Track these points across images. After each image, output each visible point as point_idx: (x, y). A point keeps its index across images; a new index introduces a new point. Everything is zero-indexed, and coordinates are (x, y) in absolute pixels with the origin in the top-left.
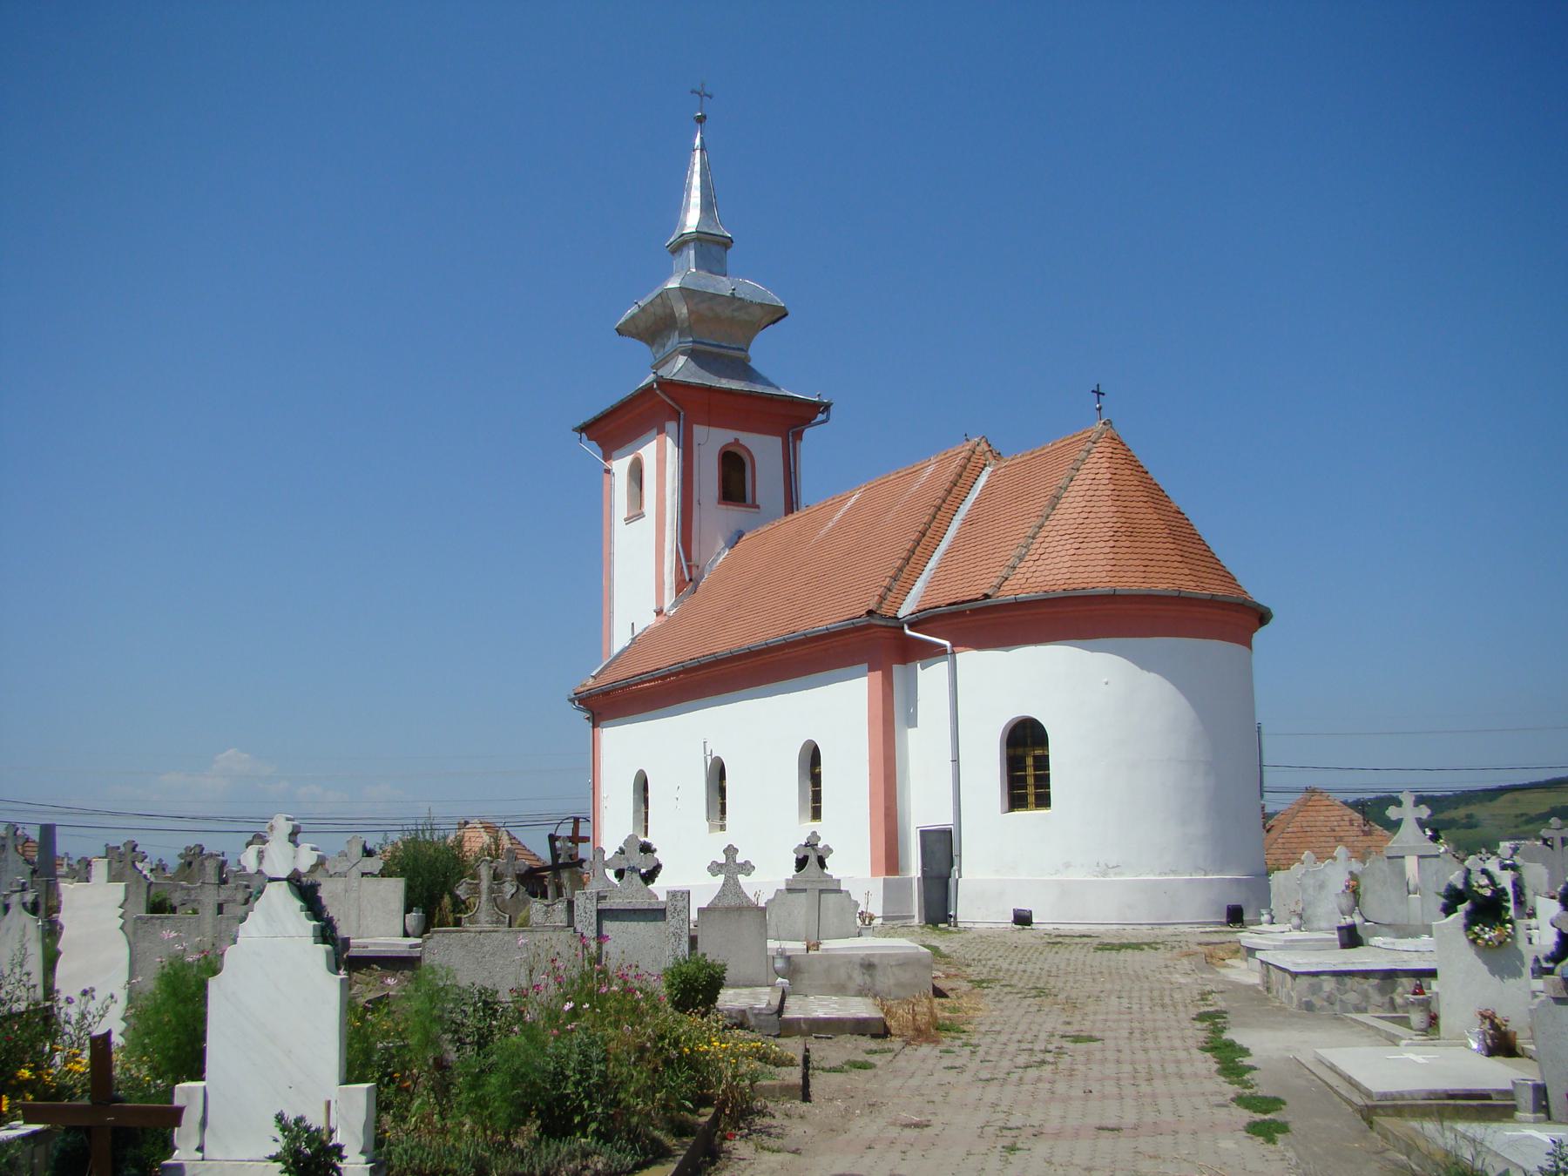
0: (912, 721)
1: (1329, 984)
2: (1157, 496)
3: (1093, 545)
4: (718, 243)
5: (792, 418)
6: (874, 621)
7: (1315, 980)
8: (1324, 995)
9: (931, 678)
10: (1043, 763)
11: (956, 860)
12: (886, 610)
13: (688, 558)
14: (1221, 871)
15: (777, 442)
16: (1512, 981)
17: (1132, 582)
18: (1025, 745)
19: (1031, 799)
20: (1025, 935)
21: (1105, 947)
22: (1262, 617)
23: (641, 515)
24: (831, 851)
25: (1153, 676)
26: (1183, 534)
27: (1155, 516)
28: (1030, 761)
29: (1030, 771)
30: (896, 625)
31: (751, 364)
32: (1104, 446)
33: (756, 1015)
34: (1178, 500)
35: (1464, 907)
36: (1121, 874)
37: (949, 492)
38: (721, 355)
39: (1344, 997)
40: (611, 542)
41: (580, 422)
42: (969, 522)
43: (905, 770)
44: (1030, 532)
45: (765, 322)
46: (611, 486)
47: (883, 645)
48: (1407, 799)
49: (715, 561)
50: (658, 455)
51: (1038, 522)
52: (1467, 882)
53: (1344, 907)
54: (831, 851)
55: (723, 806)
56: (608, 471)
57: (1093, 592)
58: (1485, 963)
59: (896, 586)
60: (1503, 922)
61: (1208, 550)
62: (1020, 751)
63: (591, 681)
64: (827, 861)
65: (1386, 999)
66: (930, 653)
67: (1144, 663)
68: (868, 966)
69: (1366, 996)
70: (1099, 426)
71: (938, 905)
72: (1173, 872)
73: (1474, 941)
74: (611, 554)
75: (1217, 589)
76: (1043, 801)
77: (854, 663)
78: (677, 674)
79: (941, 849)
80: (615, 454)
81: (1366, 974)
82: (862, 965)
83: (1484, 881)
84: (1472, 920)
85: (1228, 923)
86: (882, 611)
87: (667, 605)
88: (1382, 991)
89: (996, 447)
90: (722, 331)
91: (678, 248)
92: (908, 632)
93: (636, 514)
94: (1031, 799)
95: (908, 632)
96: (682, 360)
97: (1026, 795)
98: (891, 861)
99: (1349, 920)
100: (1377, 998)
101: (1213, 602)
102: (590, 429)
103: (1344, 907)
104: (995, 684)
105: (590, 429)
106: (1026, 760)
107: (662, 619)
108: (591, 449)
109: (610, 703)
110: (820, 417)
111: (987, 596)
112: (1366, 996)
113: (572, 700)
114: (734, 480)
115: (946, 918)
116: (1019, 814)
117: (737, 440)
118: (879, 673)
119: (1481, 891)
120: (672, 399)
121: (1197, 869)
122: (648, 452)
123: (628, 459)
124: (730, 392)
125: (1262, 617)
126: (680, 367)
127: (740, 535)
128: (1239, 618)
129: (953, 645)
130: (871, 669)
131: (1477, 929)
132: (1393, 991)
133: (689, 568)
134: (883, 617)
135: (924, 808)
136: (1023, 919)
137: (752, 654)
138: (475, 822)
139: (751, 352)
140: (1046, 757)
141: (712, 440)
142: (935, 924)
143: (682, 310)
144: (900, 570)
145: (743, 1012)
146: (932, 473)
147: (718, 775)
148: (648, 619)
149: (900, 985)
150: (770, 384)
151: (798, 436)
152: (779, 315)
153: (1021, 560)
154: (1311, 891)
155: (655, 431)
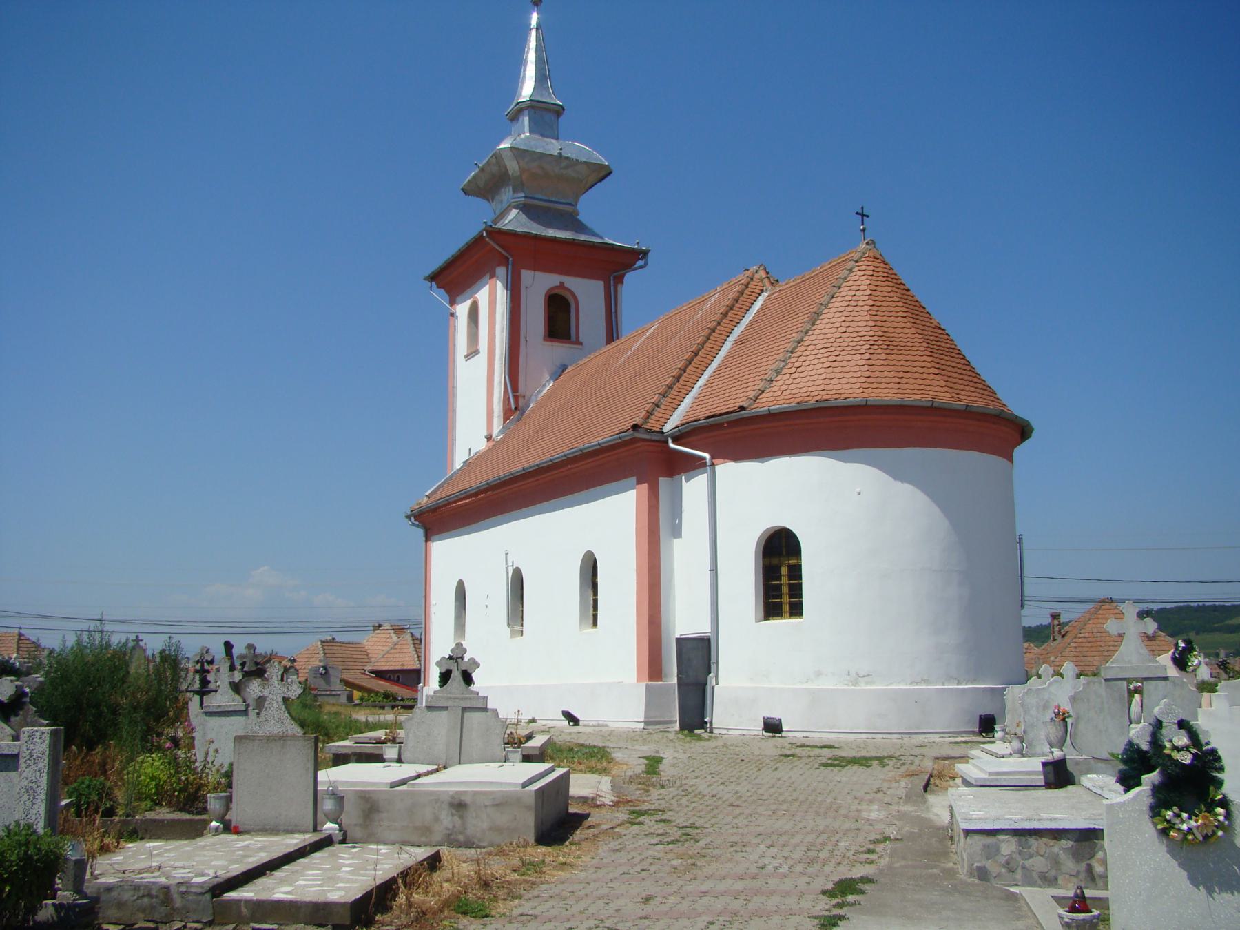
0: (677, 532)
1: (1008, 846)
2: (916, 311)
3: (849, 358)
4: (549, 110)
5: (613, 264)
6: (637, 435)
7: (989, 840)
8: (1003, 860)
9: (693, 489)
10: (796, 572)
12: (652, 424)
14: (974, 681)
15: (599, 286)
16: (1226, 896)
17: (886, 392)
18: (780, 555)
19: (786, 608)
20: (777, 740)
21: (842, 762)
22: (1023, 431)
23: (476, 352)
24: (478, 665)
25: (907, 487)
26: (941, 348)
27: (913, 331)
28: (784, 570)
29: (785, 580)
30: (660, 440)
31: (579, 217)
32: (866, 265)
33: (183, 894)
34: (938, 317)
35: (1151, 778)
37: (725, 315)
38: (549, 209)
39: (1028, 863)
40: (454, 377)
41: (428, 273)
42: (740, 342)
43: (671, 580)
44: (789, 347)
45: (591, 180)
46: (455, 327)
47: (649, 459)
48: (1130, 611)
49: (540, 391)
50: (491, 297)
51: (796, 337)
52: (1155, 741)
53: (1052, 737)
54: (478, 665)
56: (452, 315)
57: (845, 403)
58: (1182, 865)
59: (664, 402)
60: (1211, 805)
61: (972, 370)
62: (775, 561)
63: (425, 499)
64: (474, 675)
65: (1083, 866)
66: (691, 465)
67: (897, 475)
68: (459, 805)
69: (1056, 862)
70: (863, 246)
71: (694, 712)
73: (1164, 832)
75: (973, 400)
76: (796, 610)
77: (625, 477)
78: (485, 491)
79: (698, 657)
80: (458, 299)
81: (1057, 834)
82: (452, 805)
83: (1182, 739)
84: (1162, 799)
85: (980, 733)
87: (496, 431)
88: (1077, 855)
89: (774, 275)
90: (554, 188)
91: (515, 117)
92: (672, 445)
93: (473, 353)
94: (786, 608)
95: (672, 445)
96: (514, 212)
97: (780, 604)
98: (654, 669)
99: (1057, 753)
100: (1069, 865)
101: (967, 413)
102: (436, 277)
103: (1052, 737)
105: (436, 277)
106: (780, 569)
107: (491, 443)
108: (439, 296)
109: (441, 518)
110: (640, 263)
111: (742, 408)
112: (1056, 862)
113: (408, 517)
114: (559, 319)
115: (703, 725)
116: (774, 623)
117: (562, 284)
119: (1177, 756)
121: (949, 678)
122: (483, 295)
123: (468, 303)
124: (554, 240)
125: (1023, 431)
126: (514, 220)
127: (564, 368)
128: (1002, 432)
129: (713, 458)
130: (639, 482)
131: (1169, 814)
132: (1092, 856)
133: (516, 398)
134: (649, 431)
135: (686, 620)
136: (773, 727)
137: (539, 471)
138: (386, 625)
139: (580, 207)
141: (538, 284)
142: (691, 730)
143: (512, 166)
144: (670, 387)
145: (166, 889)
146: (717, 299)
147: (517, 584)
148: (482, 445)
149: (497, 829)
150: (595, 235)
151: (620, 280)
152: (603, 173)
153: (778, 373)
154: (1033, 712)
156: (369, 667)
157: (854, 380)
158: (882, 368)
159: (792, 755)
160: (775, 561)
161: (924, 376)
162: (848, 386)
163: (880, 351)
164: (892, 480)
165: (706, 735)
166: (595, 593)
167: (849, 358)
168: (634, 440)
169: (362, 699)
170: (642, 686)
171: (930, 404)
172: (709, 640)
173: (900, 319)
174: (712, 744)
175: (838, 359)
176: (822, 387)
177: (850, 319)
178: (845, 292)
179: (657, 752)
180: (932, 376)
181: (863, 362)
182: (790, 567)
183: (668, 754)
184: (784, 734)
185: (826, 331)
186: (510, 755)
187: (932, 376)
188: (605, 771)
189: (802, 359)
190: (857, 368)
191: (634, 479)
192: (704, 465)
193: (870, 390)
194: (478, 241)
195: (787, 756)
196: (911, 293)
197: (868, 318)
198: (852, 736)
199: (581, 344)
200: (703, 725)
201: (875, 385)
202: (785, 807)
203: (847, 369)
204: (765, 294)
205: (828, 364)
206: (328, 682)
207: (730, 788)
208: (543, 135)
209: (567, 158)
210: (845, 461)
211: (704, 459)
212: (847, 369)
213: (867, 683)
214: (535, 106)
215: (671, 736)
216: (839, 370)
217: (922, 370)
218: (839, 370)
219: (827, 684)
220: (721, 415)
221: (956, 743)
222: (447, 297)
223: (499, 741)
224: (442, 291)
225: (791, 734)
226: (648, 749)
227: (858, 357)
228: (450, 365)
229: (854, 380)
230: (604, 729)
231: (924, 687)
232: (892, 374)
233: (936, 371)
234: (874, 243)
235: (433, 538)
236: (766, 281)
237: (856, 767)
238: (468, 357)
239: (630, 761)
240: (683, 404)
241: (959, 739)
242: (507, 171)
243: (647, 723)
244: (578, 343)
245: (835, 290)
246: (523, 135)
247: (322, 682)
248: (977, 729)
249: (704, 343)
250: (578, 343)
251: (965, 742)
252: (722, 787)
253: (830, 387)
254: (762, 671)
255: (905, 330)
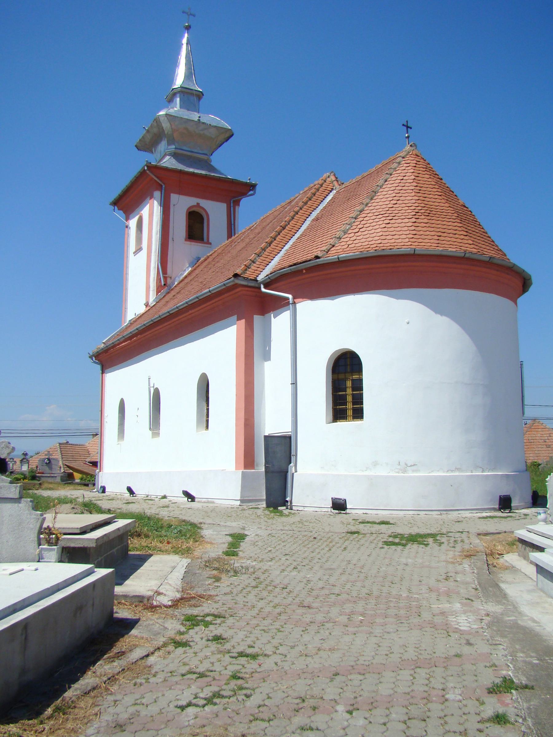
0: (267, 356)
2: (448, 194)
3: (400, 221)
9: (280, 322)
10: (358, 386)
11: (293, 459)
12: (249, 274)
13: (165, 271)
17: (428, 244)
19: (350, 413)
20: (342, 517)
25: (444, 320)
26: (466, 218)
28: (349, 384)
29: (349, 391)
31: (212, 163)
36: (417, 471)
40: (127, 268)
42: (317, 219)
47: (248, 302)
50: (151, 212)
55: (207, 421)
56: (127, 227)
59: (259, 260)
62: (341, 376)
63: (103, 345)
70: (408, 148)
71: (278, 494)
72: (458, 469)
74: (127, 274)
80: (131, 216)
85: (500, 509)
86: (246, 276)
92: (263, 290)
93: (139, 249)
94: (350, 413)
95: (263, 290)
98: (248, 461)
102: (116, 203)
104: (323, 325)
107: (148, 308)
108: (119, 215)
109: (110, 357)
110: (251, 192)
111: (317, 257)
113: (91, 357)
114: (196, 226)
115: (284, 503)
116: (341, 424)
117: (198, 204)
118: (243, 321)
120: (158, 177)
121: (476, 467)
122: (145, 212)
123: (137, 218)
124: (193, 174)
125: (523, 283)
126: (168, 162)
128: (513, 282)
129: (294, 298)
130: (239, 319)
133: (165, 278)
134: (246, 279)
135: (273, 421)
136: (339, 506)
140: (361, 380)
141: (182, 204)
143: (166, 125)
148: (143, 309)
151: (237, 203)
152: (229, 135)
153: (345, 233)
155: (149, 198)
156: (88, 460)
157: (404, 236)
158: (425, 229)
159: (358, 532)
160: (341, 376)
161: (457, 236)
162: (400, 241)
163: (423, 217)
164: (432, 313)
165: (286, 512)
166: (208, 405)
167: (400, 221)
168: (235, 286)
169: (82, 479)
170: (240, 472)
171: (463, 255)
172: (290, 437)
173: (436, 197)
174: (291, 519)
175: (391, 222)
176: (379, 241)
177: (400, 195)
178: (395, 178)
179: (244, 529)
180: (462, 237)
181: (410, 224)
182: (353, 380)
183: (251, 532)
184: (348, 511)
185: (380, 204)
186: (45, 554)
187: (462, 237)
188: (186, 552)
189: (363, 222)
190: (406, 228)
191: (235, 317)
192: (288, 304)
193: (416, 244)
194: (142, 174)
195: (352, 533)
196: (443, 181)
197: (413, 194)
198: (402, 513)
199: (210, 244)
200: (284, 503)
201: (420, 240)
202: (359, 608)
203: (399, 229)
204: (334, 192)
205: (384, 225)
206: (51, 468)
207: (302, 574)
208: (188, 110)
209: (203, 123)
210: (397, 298)
211: (288, 299)
212: (399, 229)
213: (413, 471)
214: (184, 92)
215: (259, 512)
216: (392, 229)
217: (455, 232)
218: (392, 229)
219: (382, 472)
220: (301, 263)
221: (483, 518)
222: (124, 215)
223: (33, 536)
224: (121, 212)
225: (353, 511)
226: (235, 526)
227: (407, 220)
228: (125, 259)
229: (404, 236)
230: (210, 505)
231: (457, 474)
232: (433, 233)
233: (466, 234)
234: (416, 146)
235: (106, 371)
236: (335, 183)
237: (415, 546)
238: (136, 253)
239: (215, 540)
240: (273, 262)
241: (484, 514)
242: (163, 131)
243: (242, 501)
244: (208, 243)
245: (388, 176)
246: (176, 108)
247: (46, 469)
248: (497, 506)
249: (290, 221)
250: (208, 243)
251: (490, 517)
252: (294, 573)
253: (386, 241)
254: (331, 462)
255: (440, 203)
